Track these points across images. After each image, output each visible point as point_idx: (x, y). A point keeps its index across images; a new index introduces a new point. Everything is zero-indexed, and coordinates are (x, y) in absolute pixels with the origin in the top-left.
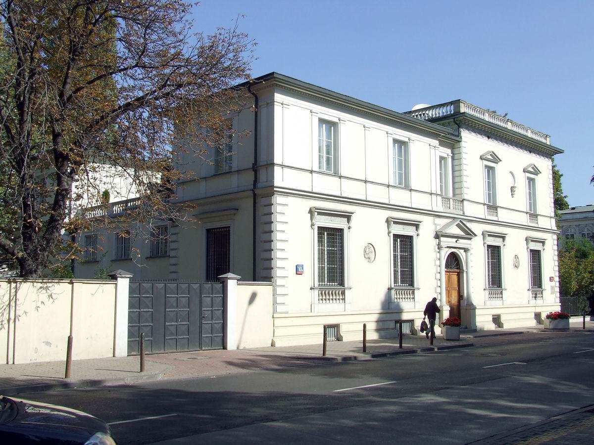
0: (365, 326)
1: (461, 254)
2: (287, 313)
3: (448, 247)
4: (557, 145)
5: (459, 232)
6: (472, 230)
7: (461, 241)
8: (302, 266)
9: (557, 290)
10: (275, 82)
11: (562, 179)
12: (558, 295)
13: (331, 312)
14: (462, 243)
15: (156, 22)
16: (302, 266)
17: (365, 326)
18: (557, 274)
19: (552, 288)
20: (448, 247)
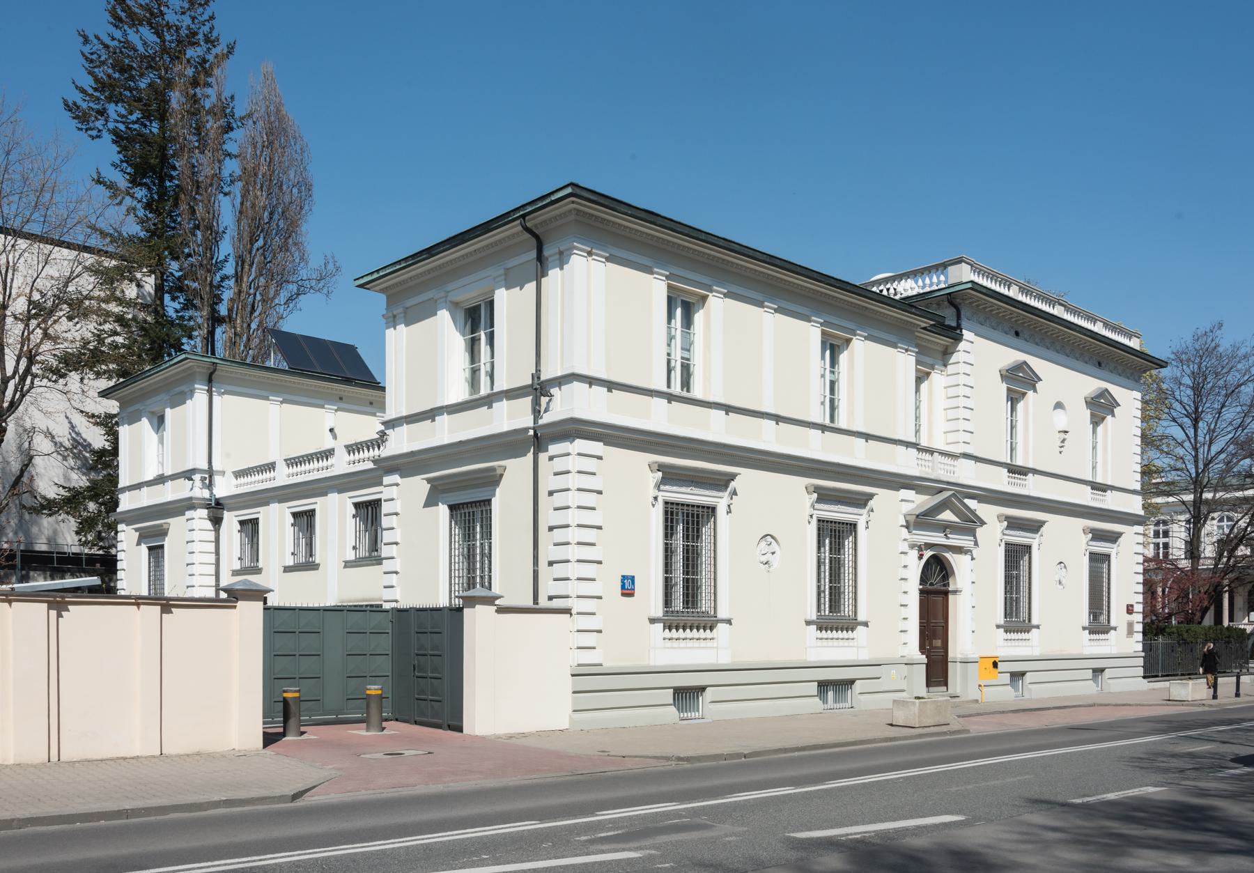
14: (956, 540)
16: (623, 595)
18: (1140, 598)
19: (1130, 625)
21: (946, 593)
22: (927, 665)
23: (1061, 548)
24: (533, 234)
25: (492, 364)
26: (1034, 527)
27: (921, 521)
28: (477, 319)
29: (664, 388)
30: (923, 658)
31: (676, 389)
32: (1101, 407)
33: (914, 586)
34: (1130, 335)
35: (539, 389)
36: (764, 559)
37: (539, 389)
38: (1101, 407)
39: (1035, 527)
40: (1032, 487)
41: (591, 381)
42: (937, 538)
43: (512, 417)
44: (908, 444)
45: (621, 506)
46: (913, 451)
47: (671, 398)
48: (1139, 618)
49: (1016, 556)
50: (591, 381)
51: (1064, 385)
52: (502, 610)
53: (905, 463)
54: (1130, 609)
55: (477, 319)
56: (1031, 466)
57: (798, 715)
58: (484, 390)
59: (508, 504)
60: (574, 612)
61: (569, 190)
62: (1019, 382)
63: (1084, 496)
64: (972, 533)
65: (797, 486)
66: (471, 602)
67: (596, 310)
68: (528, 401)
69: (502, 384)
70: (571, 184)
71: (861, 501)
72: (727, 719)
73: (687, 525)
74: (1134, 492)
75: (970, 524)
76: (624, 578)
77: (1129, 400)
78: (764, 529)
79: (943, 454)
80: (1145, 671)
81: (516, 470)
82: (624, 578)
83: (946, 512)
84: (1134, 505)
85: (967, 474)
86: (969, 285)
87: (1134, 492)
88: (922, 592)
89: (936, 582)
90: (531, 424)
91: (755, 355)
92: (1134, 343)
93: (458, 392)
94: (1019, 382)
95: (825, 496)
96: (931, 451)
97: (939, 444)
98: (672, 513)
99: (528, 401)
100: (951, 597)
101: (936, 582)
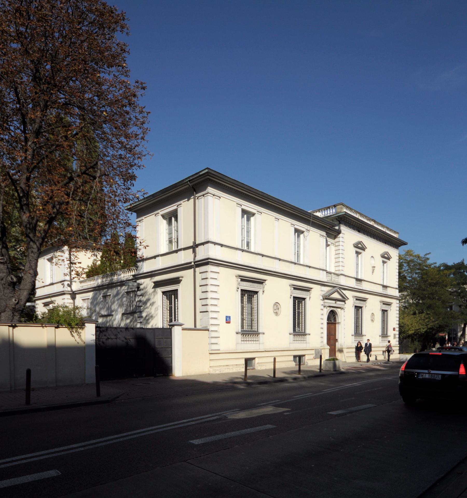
0: (275, 359)
1: (338, 311)
2: (219, 350)
3: (330, 307)
4: (404, 239)
5: (339, 297)
6: (148, 257)
7: (338, 302)
8: (230, 317)
9: (397, 336)
10: (208, 177)
11: (220, 247)
12: (398, 339)
13: (249, 346)
14: (339, 304)
15: (85, 139)
16: (230, 317)
17: (275, 359)
18: (398, 326)
19: (395, 335)
20: (330, 307)
21: (335, 324)
22: (330, 349)
23: (373, 306)
24: (193, 186)
25: (177, 239)
26: (364, 300)
27: (326, 298)
28: (172, 217)
29: (240, 247)
30: (329, 347)
31: (246, 248)
32: (386, 257)
33: (325, 321)
34: (395, 232)
35: (194, 247)
36: (275, 311)
37: (194, 247)
38: (386, 257)
39: (364, 300)
40: (365, 286)
41: (215, 244)
42: (332, 303)
43: (185, 257)
44: (323, 270)
45: (225, 288)
46: (325, 272)
47: (243, 251)
48: (398, 333)
49: (358, 309)
50: (215, 244)
51: (375, 248)
52: (183, 329)
53: (322, 277)
54: (394, 329)
55: (172, 217)
56: (363, 279)
57: (286, 364)
58: (174, 248)
59: (185, 290)
60: (210, 330)
61: (207, 171)
62: (360, 248)
63: (379, 289)
64: (344, 301)
65: (287, 283)
66: (173, 325)
67: (218, 214)
68: (191, 250)
69: (181, 246)
70: (207, 168)
71: (308, 290)
72: (263, 366)
73: (249, 296)
74: (396, 289)
75: (344, 299)
76: (227, 317)
77: (394, 253)
78: (275, 295)
79: (334, 274)
80: (399, 351)
81: (187, 275)
82: (227, 317)
83: (335, 294)
84: (396, 293)
85: (343, 281)
86: (344, 213)
87: (396, 289)
88: (328, 323)
89: (332, 318)
90: (192, 260)
91: (272, 234)
92: (395, 235)
93: (164, 249)
94: (360, 248)
95: (296, 288)
96: (330, 273)
97: (333, 270)
98: (243, 292)
99: (191, 250)
100: (337, 325)
101: (332, 318)
